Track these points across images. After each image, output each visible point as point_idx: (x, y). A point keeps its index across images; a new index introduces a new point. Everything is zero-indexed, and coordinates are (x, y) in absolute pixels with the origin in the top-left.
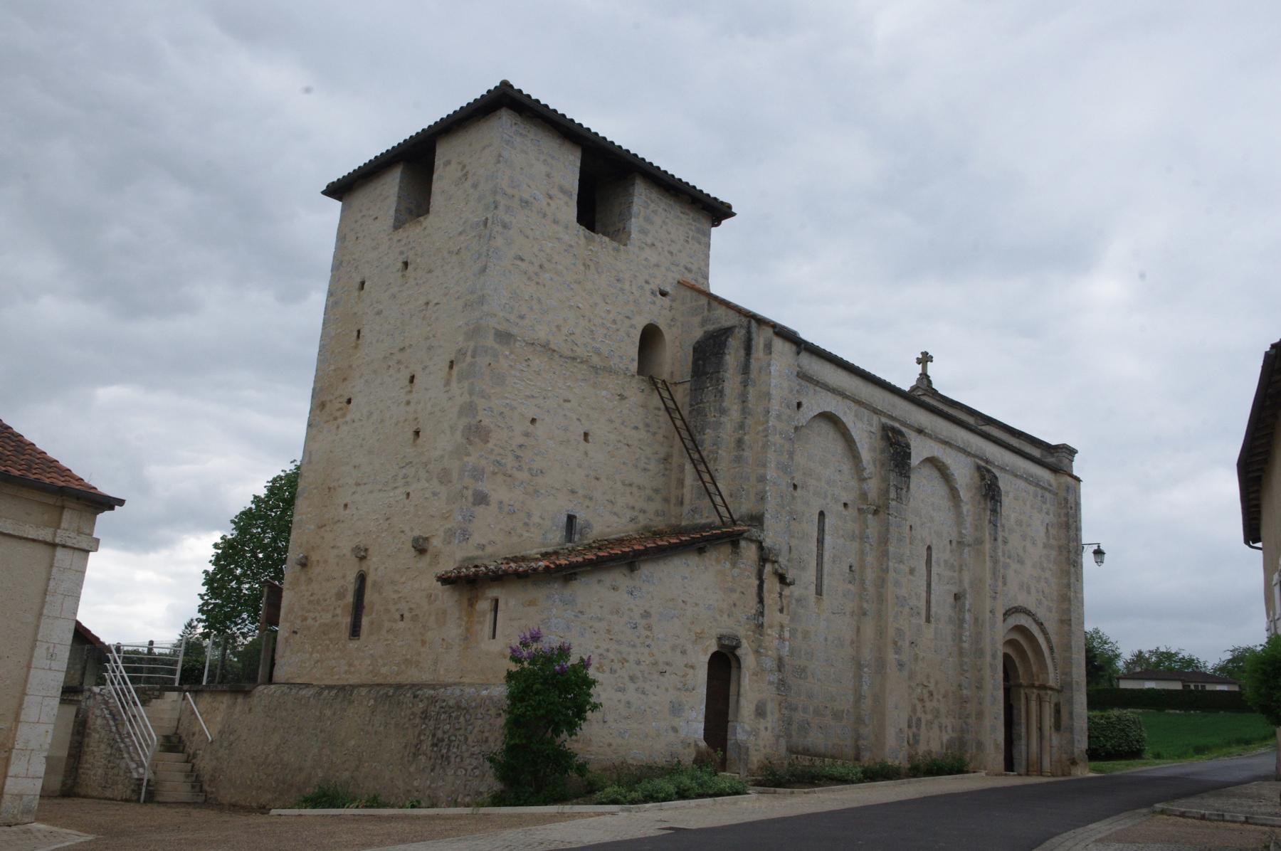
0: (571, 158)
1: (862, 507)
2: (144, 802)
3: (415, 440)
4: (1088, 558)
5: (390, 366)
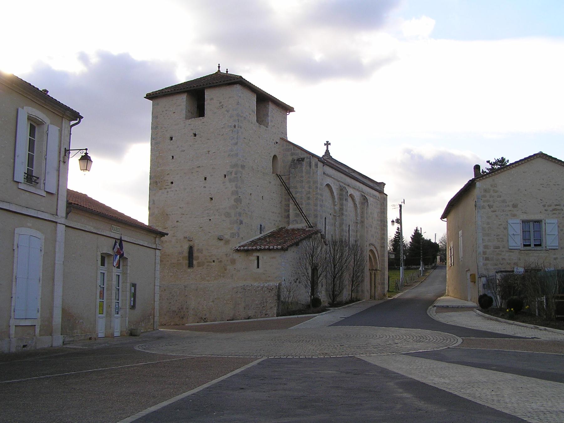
1: (335, 214)
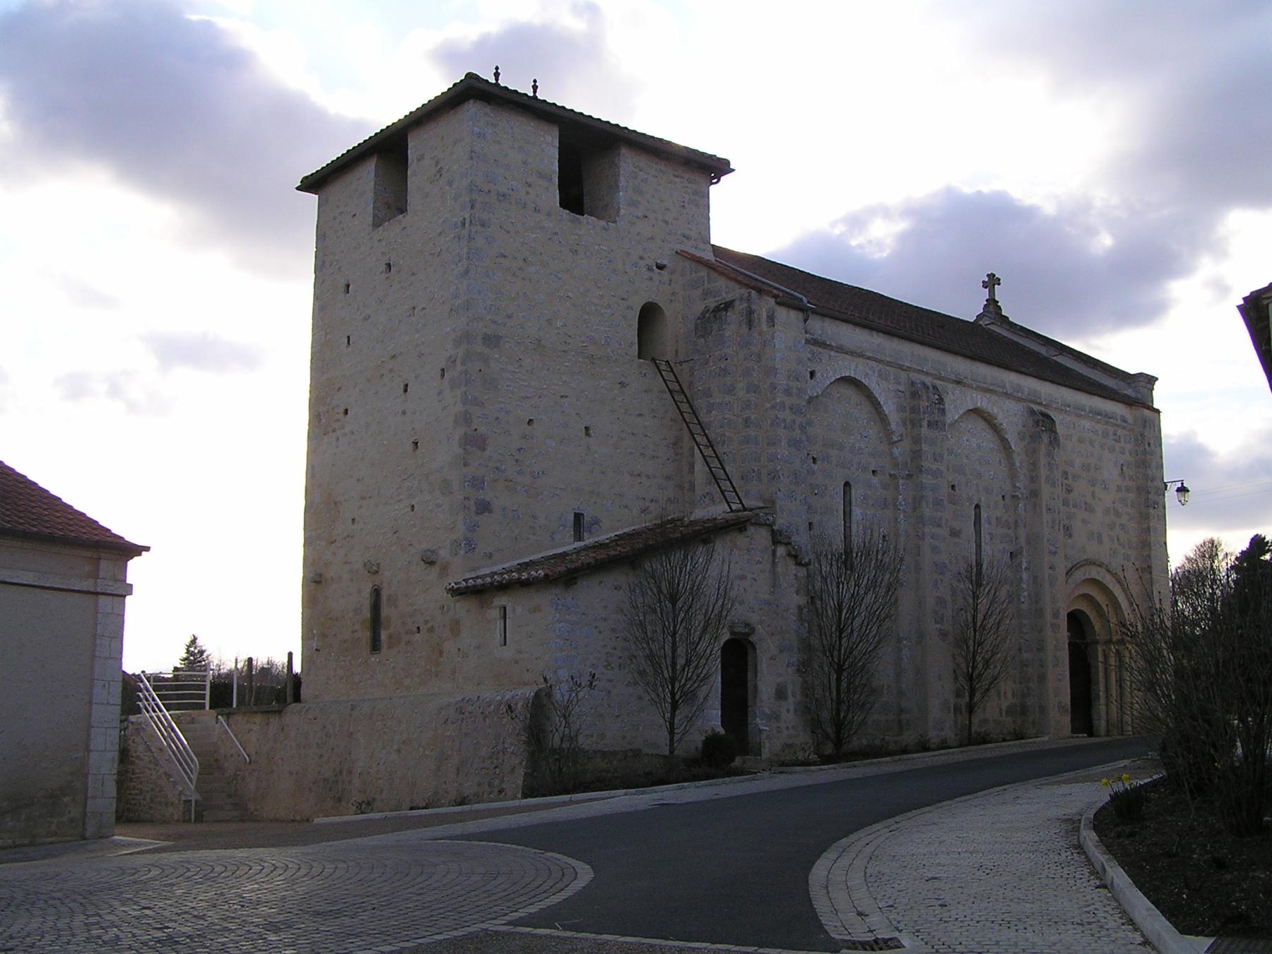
0: (549, 139)
1: (892, 472)
2: (195, 822)
3: (414, 450)
4: (1171, 496)
5: (383, 375)
